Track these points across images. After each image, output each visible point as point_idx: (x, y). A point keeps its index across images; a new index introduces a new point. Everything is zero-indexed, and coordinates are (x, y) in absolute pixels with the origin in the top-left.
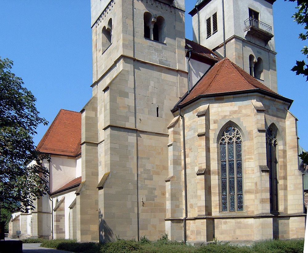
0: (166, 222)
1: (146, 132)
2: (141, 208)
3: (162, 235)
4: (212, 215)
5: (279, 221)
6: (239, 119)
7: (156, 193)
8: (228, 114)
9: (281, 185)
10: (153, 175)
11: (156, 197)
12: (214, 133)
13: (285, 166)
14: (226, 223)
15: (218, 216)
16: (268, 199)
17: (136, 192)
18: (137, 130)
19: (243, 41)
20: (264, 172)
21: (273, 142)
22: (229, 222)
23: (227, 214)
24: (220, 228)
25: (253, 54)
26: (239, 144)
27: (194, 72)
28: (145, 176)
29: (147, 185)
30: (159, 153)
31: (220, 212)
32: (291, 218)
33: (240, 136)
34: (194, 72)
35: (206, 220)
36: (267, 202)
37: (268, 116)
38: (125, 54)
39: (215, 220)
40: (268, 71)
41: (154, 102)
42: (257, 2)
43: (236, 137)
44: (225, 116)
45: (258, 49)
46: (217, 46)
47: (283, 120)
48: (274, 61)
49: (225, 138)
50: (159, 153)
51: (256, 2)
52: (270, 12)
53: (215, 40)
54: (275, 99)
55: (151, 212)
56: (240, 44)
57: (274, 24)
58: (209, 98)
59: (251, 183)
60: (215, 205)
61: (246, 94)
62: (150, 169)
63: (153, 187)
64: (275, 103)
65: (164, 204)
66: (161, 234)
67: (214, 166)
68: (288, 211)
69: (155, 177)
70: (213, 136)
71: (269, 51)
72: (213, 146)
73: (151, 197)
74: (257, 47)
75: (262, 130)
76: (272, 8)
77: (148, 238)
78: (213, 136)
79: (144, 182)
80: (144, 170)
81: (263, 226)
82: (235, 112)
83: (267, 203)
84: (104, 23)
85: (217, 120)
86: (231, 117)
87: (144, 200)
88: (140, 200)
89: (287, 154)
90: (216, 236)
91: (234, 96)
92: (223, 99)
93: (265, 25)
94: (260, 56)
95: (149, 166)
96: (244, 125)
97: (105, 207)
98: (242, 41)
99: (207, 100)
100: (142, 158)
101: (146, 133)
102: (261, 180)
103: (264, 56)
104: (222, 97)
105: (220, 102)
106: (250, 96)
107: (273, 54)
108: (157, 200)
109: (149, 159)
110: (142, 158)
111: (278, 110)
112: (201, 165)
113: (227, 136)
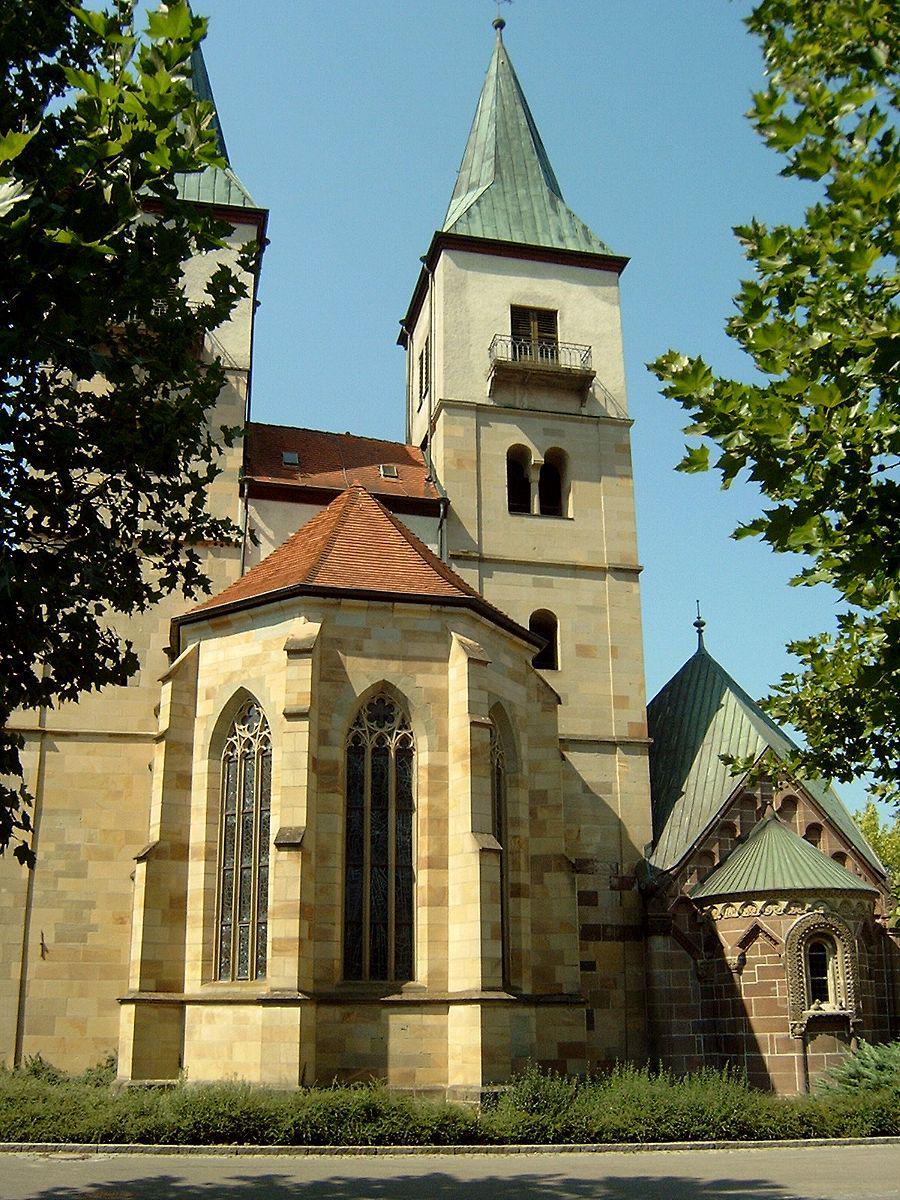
0: (124, 1007)
1: (76, 734)
2: (35, 962)
3: (106, 1052)
4: (185, 992)
5: (391, 1016)
6: (260, 680)
7: (95, 916)
8: (238, 667)
9: (422, 887)
10: (90, 863)
11: (94, 928)
13: (439, 821)
14: (211, 1018)
15: (197, 996)
16: (294, 939)
17: (23, 914)
18: (45, 733)
19: (479, 409)
20: (286, 848)
21: (393, 743)
22: (219, 1015)
23: (220, 990)
24: (196, 1037)
25: (526, 441)
27: (267, 537)
28: (60, 865)
29: (64, 893)
30: (119, 794)
31: (204, 981)
32: (453, 1008)
34: (267, 537)
35: (134, 1006)
36: (289, 950)
37: (361, 661)
39: (188, 1008)
40: (595, 485)
42: (551, 278)
44: (233, 674)
45: (549, 421)
47: (436, 666)
48: (626, 449)
49: (364, 732)
50: (119, 794)
51: (543, 281)
52: (605, 299)
54: (391, 604)
55: (72, 978)
56: (470, 421)
57: (622, 331)
58: (196, 625)
60: (192, 958)
62: (77, 842)
63: (83, 899)
64: (395, 616)
65: (120, 951)
66: (102, 1050)
67: (198, 832)
68: (450, 982)
69: (95, 869)
70: (202, 736)
71: (600, 420)
72: (200, 766)
73: (76, 931)
74: (544, 417)
75: (295, 711)
76: (617, 284)
77: (50, 1059)
78: (202, 736)
79: (56, 883)
80: (60, 847)
81: (268, 1035)
82: (254, 660)
83: (290, 953)
85: (213, 688)
86: (244, 677)
87: (49, 941)
88: (34, 941)
89: (450, 778)
90: (185, 1063)
91: (251, 611)
92: (228, 624)
93: (573, 347)
94: (553, 442)
95: (75, 836)
96: (272, 700)
98: (477, 411)
99: (194, 630)
100: (54, 812)
101: (77, 738)
103: (573, 440)
104: (224, 619)
105: (222, 632)
106: (289, 607)
107: (622, 425)
108: (94, 940)
109: (79, 812)
110: (54, 812)
111: (411, 635)
113: (369, 728)
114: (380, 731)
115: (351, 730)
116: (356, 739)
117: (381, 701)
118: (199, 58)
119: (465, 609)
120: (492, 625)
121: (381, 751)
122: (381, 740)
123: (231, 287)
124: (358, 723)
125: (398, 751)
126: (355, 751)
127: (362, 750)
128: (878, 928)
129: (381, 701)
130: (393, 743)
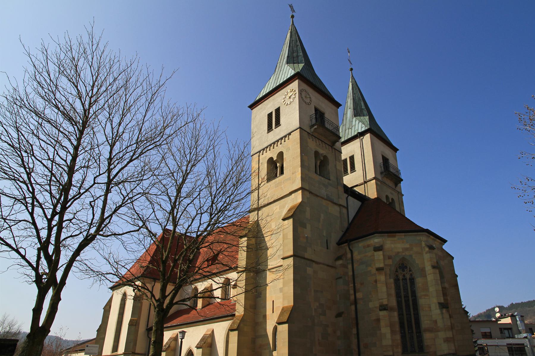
6: (411, 256)
8: (401, 250)
12: (390, 269)
21: (408, 276)
26: (412, 281)
33: (413, 273)
38: (303, 187)
41: (325, 235)
43: (409, 273)
44: (398, 253)
46: (357, 184)
53: (353, 179)
59: (253, 288)
61: (416, 233)
82: (407, 249)
84: (273, 154)
86: (404, 254)
97: (47, 292)
102: (443, 318)
112: (381, 301)
114: (403, 273)
115: (395, 274)
116: (397, 276)
117: (403, 264)
118: (289, 53)
119: (375, 235)
120: (403, 234)
121: (405, 279)
122: (404, 276)
123: (176, 258)
124: (397, 271)
125: (410, 279)
126: (397, 280)
127: (399, 280)
128: (510, 353)
129: (403, 264)
130: (408, 276)
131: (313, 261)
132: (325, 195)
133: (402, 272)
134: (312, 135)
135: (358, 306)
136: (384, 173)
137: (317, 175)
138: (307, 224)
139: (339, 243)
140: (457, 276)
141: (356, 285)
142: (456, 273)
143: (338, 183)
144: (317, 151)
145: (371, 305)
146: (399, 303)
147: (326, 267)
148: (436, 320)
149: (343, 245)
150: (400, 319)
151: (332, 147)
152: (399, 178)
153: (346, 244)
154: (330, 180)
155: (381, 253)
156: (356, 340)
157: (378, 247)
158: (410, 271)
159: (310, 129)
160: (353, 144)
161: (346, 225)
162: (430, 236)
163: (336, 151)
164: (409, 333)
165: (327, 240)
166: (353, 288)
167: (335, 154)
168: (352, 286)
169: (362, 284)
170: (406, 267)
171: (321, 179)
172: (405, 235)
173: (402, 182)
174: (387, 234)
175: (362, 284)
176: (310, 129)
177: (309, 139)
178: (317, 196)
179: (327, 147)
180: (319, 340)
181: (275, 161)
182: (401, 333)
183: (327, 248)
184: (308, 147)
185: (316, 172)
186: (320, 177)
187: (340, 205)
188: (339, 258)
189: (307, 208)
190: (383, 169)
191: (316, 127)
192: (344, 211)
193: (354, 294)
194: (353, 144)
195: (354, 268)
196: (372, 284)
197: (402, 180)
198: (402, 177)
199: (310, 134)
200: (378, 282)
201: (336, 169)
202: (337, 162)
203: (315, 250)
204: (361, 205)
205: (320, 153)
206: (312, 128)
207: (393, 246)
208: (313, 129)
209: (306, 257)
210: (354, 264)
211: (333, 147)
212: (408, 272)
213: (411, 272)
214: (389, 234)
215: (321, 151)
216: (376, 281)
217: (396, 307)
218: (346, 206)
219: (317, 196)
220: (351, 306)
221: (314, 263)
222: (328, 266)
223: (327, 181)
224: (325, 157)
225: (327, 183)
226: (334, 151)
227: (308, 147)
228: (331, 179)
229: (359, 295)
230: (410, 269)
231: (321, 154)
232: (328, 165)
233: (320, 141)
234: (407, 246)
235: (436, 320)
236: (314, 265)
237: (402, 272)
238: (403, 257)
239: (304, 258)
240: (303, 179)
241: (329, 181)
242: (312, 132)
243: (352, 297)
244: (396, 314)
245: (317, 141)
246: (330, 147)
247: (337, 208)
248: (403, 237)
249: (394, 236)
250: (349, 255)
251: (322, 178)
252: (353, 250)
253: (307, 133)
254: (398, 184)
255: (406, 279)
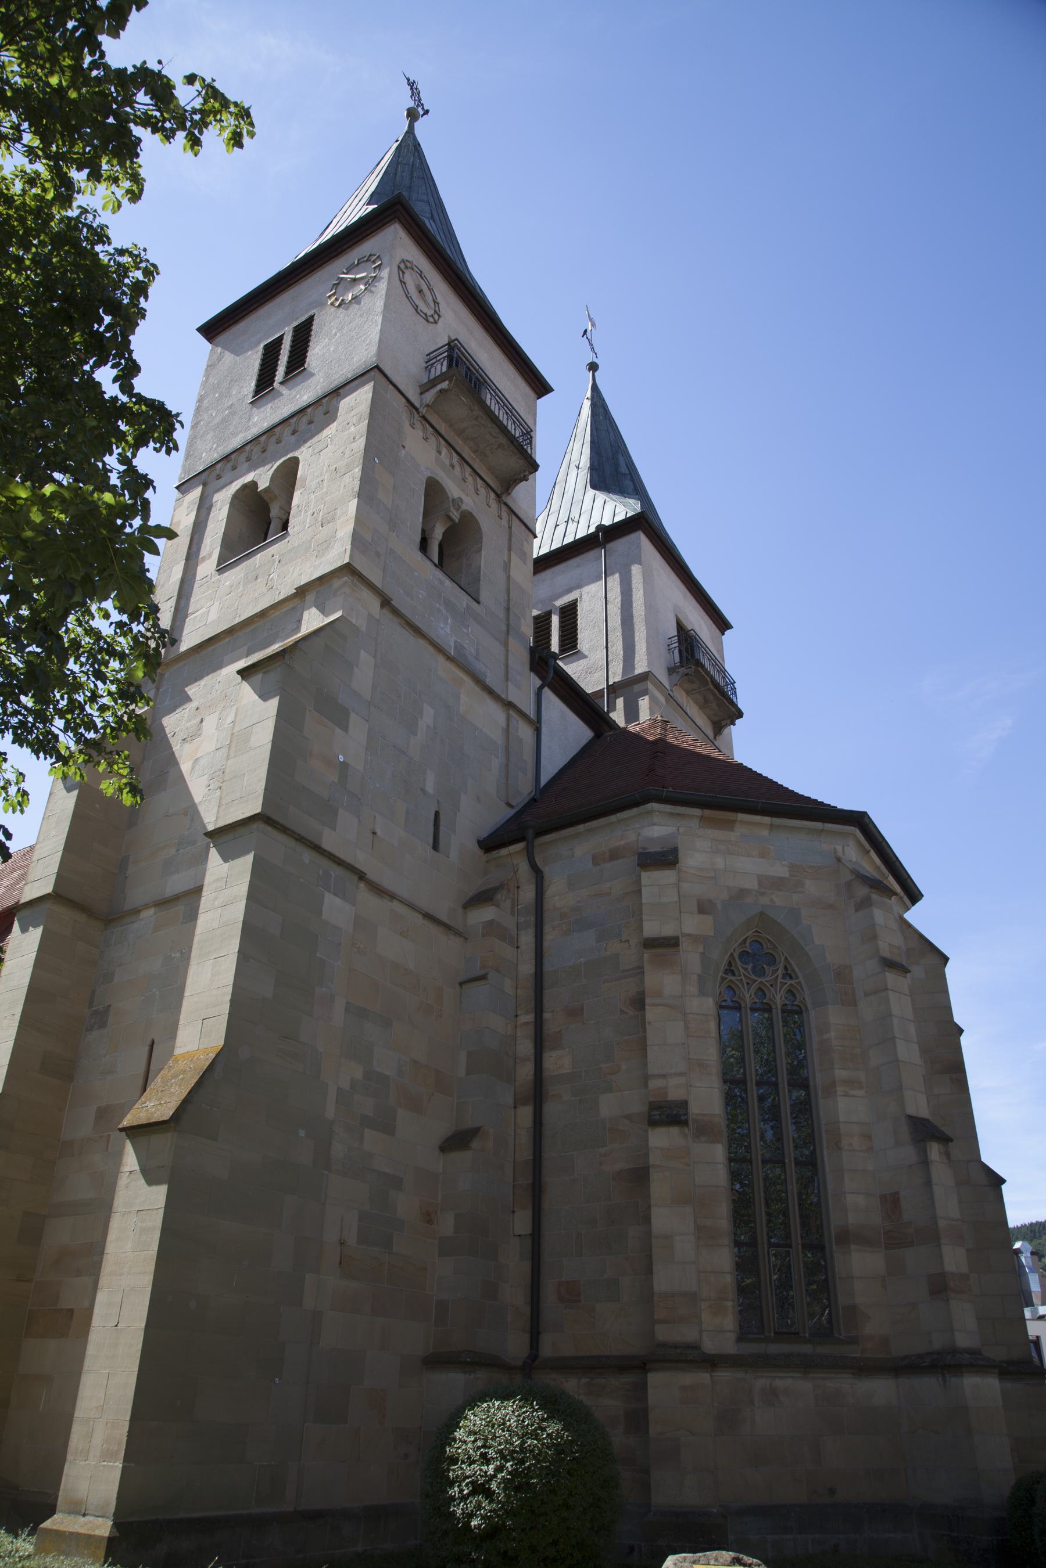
8: (752, 884)
21: (779, 998)
26: (795, 1013)
44: (742, 893)
61: (818, 825)
82: (778, 884)
115: (723, 979)
119: (650, 806)
120: (767, 820)
124: (730, 970)
130: (779, 998)
131: (361, 876)
132: (452, 644)
133: (753, 977)
134: (424, 418)
135: (550, 1109)
136: (682, 670)
137: (428, 562)
138: (353, 716)
139: (490, 844)
140: (961, 1031)
141: (547, 1015)
142: (957, 1019)
143: (508, 625)
144: (437, 482)
145: (608, 1106)
146: (731, 1100)
147: (418, 919)
148: (897, 1193)
149: (504, 851)
150: (735, 1176)
151: (498, 496)
152: (735, 706)
153: (521, 846)
154: (478, 602)
155: (666, 876)
156: (526, 1266)
157: (657, 853)
158: (788, 975)
159: (421, 394)
160: (577, 566)
161: (525, 789)
162: (868, 852)
163: (514, 517)
164: (771, 1245)
165: (437, 814)
166: (531, 1030)
167: (510, 528)
168: (527, 1023)
169: (575, 1013)
170: (772, 960)
171: (442, 583)
172: (772, 826)
173: (738, 722)
174: (697, 812)
175: (575, 1013)
176: (421, 394)
177: (412, 426)
178: (417, 631)
179: (483, 491)
180: (342, 1243)
181: (263, 495)
182: (737, 1244)
183: (435, 846)
184: (403, 452)
185: (424, 545)
186: (439, 574)
187: (509, 705)
188: (482, 898)
189: (363, 653)
190: (677, 659)
191: (445, 385)
192: (525, 732)
193: (532, 1058)
194: (577, 566)
195: (546, 944)
196: (622, 1011)
197: (740, 715)
198: (742, 703)
199: (417, 409)
200: (648, 1001)
201: (509, 577)
202: (509, 683)
203: (374, 833)
204: (590, 741)
205: (449, 495)
206: (428, 390)
207: (720, 862)
208: (430, 396)
209: (326, 845)
210: (547, 929)
211: (504, 498)
212: (779, 980)
213: (792, 982)
214: (707, 812)
215: (453, 490)
216: (639, 1002)
217: (722, 1122)
218: (532, 715)
219: (417, 631)
220: (515, 1107)
221: (362, 885)
222: (427, 916)
223: (464, 600)
224: (468, 518)
225: (465, 606)
226: (505, 514)
227: (403, 452)
228: (481, 599)
229: (557, 1062)
230: (786, 968)
231: (453, 500)
232: (480, 550)
233: (455, 455)
234: (780, 870)
235: (897, 1193)
236: (363, 893)
237: (753, 977)
238: (762, 913)
239: (317, 848)
240: (356, 538)
241: (475, 603)
242: (428, 406)
243: (526, 1072)
244: (719, 1152)
245: (444, 451)
246: (492, 495)
247: (498, 714)
248: (765, 833)
249: (730, 825)
250: (528, 894)
251: (448, 583)
252: (546, 870)
253: (404, 400)
254: (726, 725)
255: (768, 1009)
